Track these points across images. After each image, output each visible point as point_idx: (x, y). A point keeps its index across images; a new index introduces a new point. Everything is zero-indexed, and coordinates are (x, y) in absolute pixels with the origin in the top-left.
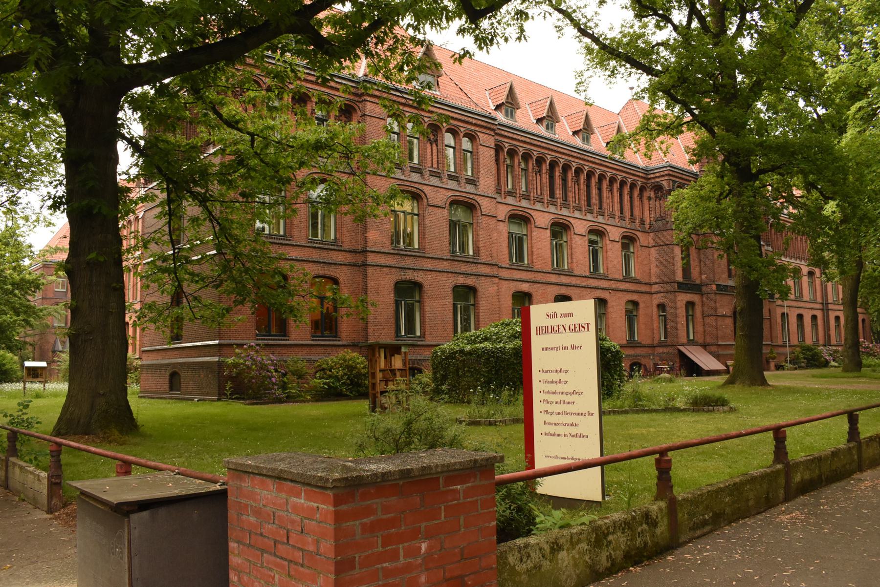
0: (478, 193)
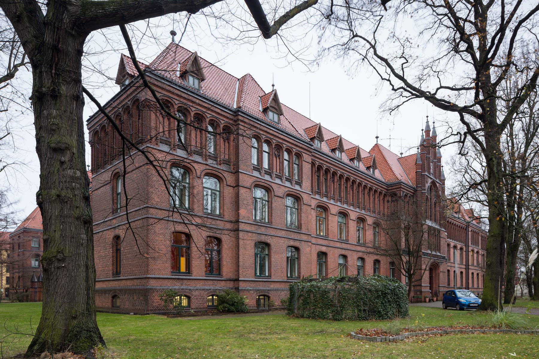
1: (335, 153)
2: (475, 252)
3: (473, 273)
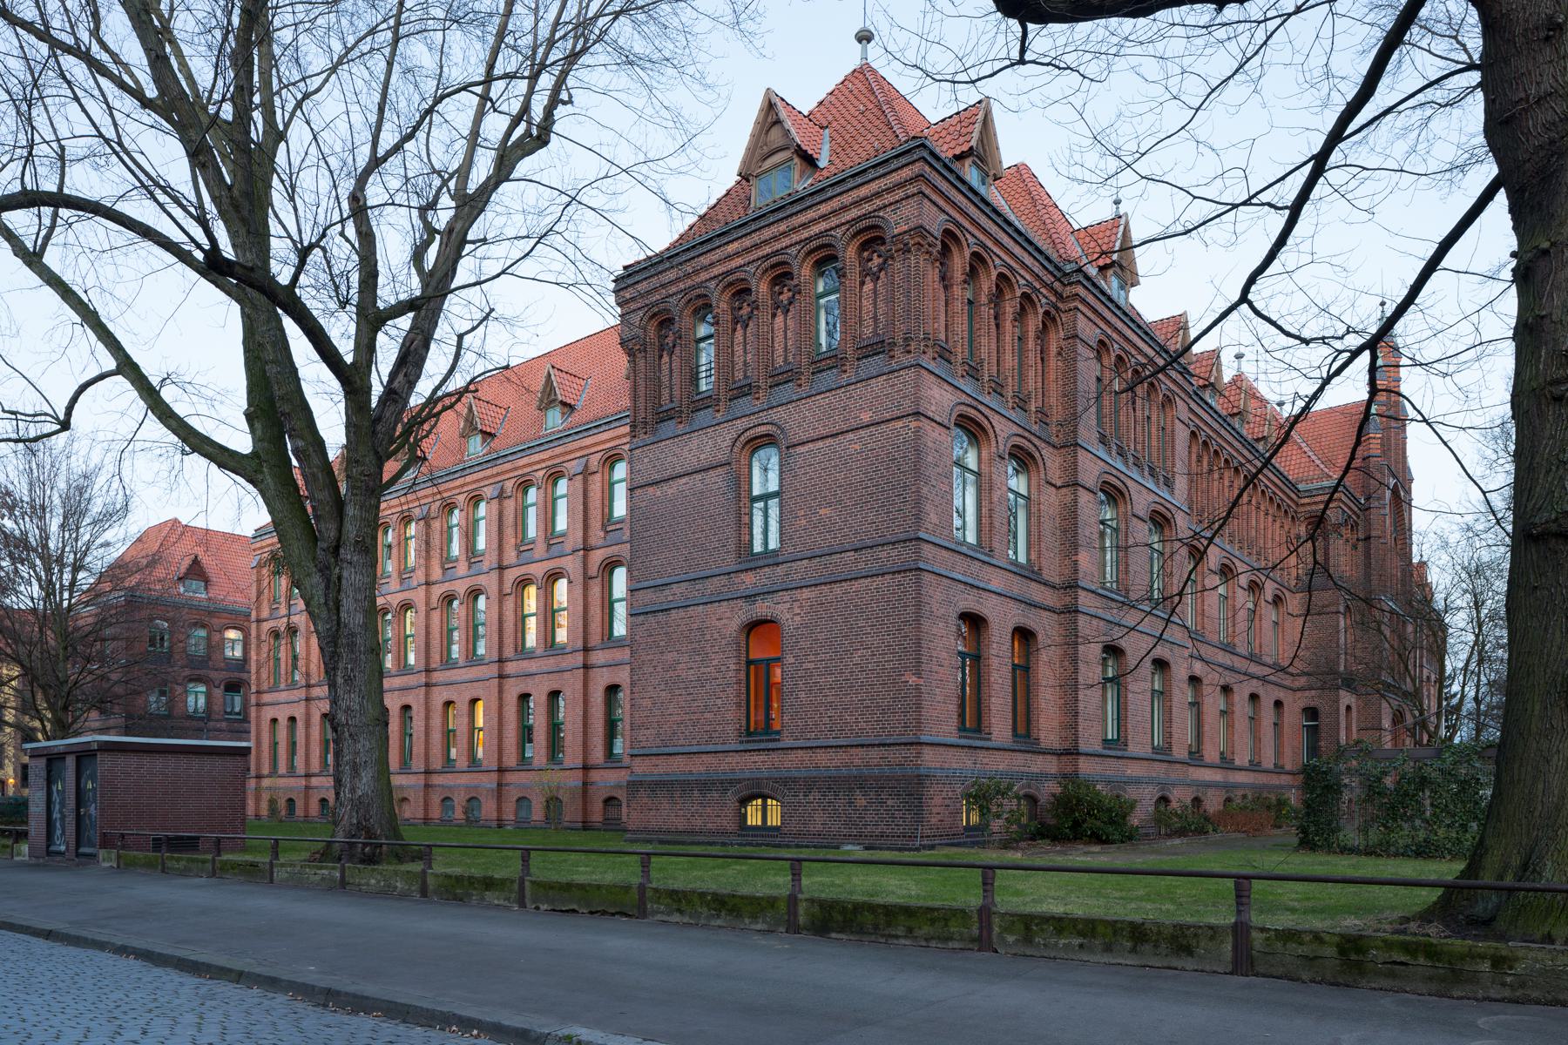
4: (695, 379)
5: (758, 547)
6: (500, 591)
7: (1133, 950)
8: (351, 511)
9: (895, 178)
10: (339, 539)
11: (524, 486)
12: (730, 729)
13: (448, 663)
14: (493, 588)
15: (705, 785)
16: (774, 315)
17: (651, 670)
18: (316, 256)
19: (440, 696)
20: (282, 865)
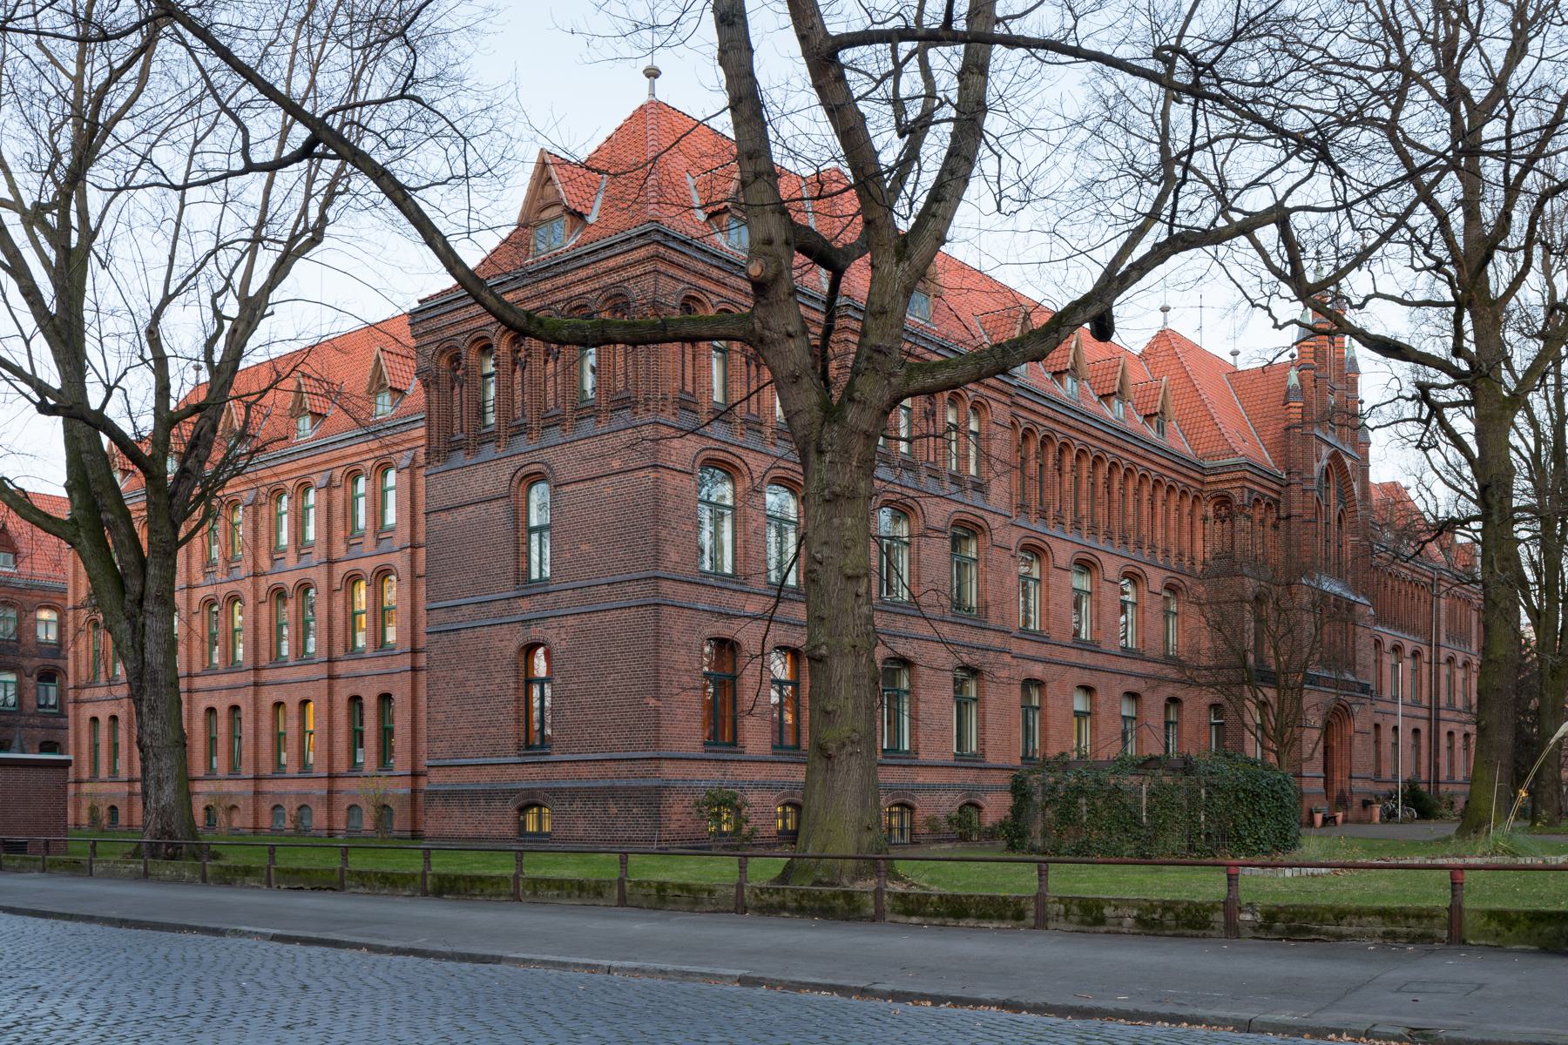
0: (989, 508)
1: (1062, 384)
2: (1460, 664)
3: (1450, 734)
4: (481, 412)
5: (535, 575)
6: (330, 586)
7: (580, 896)
8: (152, 570)
9: (636, 255)
10: (142, 593)
11: (353, 476)
12: (511, 742)
13: (277, 661)
14: (322, 583)
15: (490, 795)
16: (546, 362)
17: (444, 685)
18: (116, 391)
19: (269, 696)
20: (100, 861)
